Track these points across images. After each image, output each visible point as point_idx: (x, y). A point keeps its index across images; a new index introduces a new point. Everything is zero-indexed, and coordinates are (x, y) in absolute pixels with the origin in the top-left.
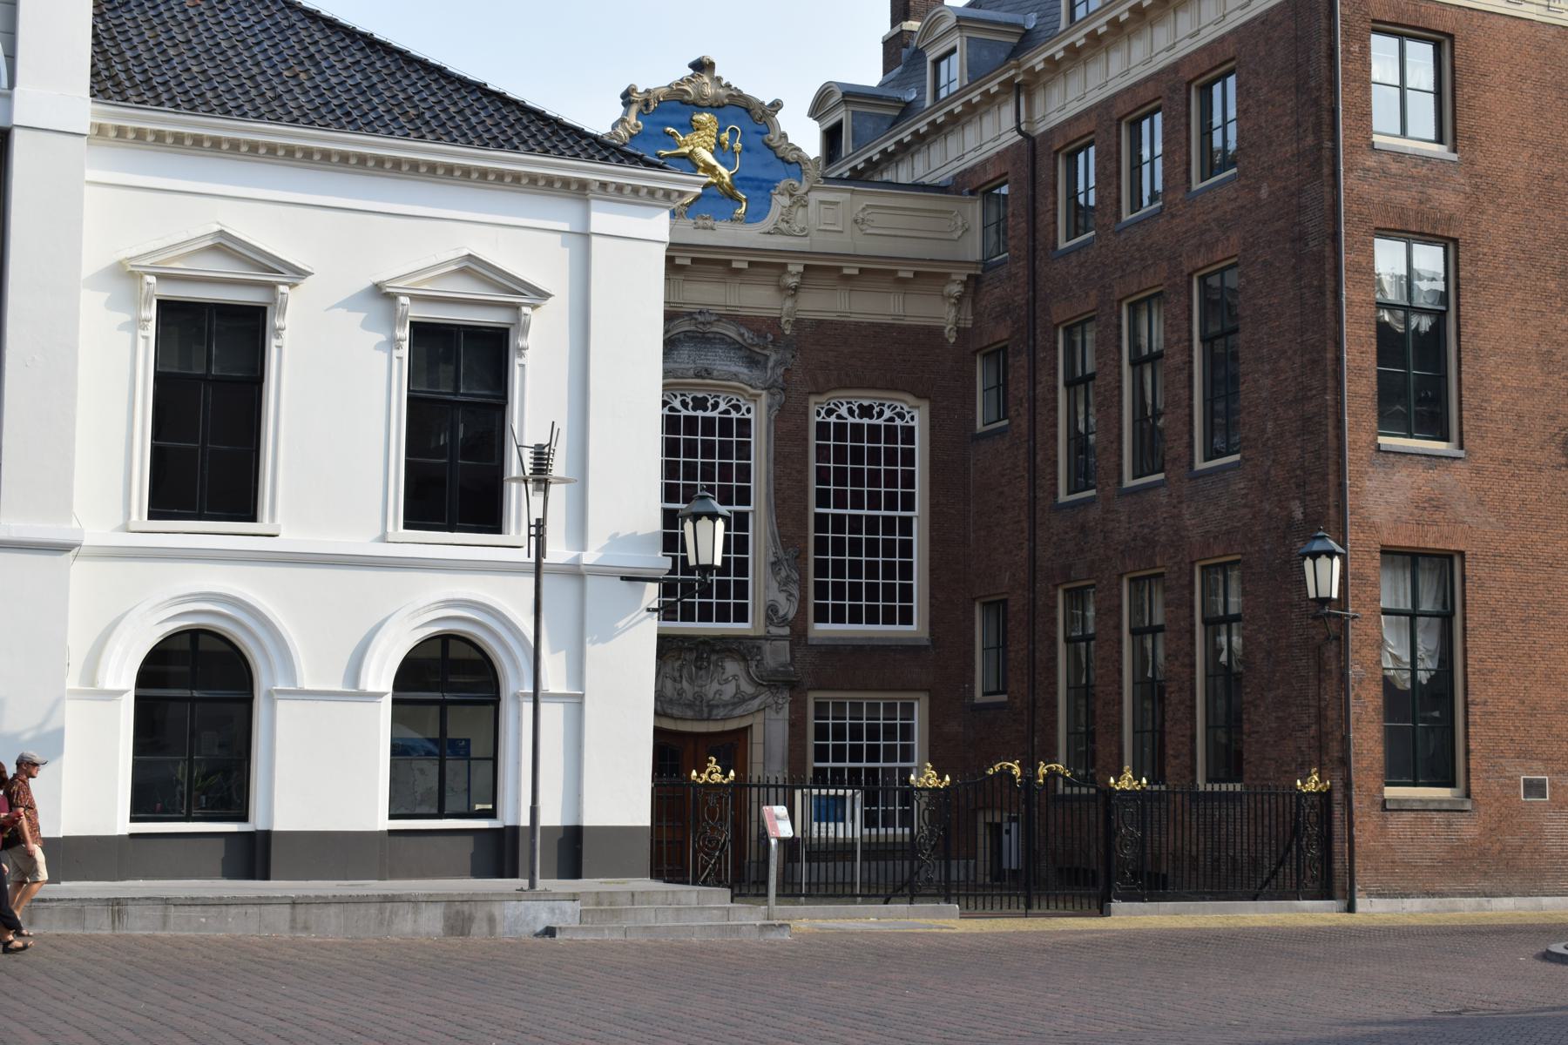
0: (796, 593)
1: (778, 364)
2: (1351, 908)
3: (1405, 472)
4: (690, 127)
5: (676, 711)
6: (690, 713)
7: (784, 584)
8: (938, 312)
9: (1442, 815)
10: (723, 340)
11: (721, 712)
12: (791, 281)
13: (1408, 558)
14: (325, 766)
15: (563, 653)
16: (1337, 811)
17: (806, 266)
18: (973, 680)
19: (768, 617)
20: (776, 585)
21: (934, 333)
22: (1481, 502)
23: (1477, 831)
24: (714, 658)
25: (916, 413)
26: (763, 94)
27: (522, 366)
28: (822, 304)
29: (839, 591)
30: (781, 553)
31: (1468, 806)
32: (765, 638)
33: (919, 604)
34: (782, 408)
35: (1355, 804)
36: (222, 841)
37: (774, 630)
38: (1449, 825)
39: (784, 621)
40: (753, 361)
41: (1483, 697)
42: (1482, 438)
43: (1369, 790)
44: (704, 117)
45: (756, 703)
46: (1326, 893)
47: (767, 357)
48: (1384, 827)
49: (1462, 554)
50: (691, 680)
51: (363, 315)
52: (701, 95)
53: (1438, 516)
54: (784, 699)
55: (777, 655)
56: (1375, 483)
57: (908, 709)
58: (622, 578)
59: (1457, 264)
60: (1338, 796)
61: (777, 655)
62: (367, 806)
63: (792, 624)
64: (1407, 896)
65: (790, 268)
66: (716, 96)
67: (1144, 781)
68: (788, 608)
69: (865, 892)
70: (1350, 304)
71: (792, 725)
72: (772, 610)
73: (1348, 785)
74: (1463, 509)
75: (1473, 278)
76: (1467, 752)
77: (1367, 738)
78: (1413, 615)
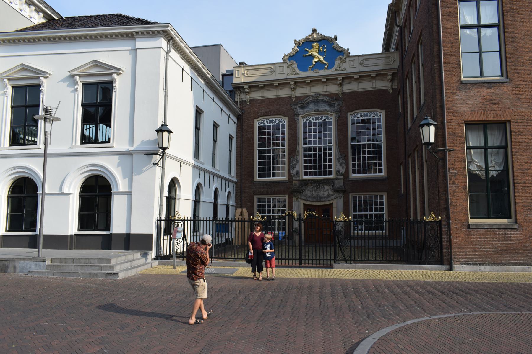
0: (345, 166)
1: (338, 105)
2: (451, 269)
3: (476, 91)
4: (311, 47)
5: (311, 200)
6: (315, 200)
7: (341, 164)
8: (382, 85)
9: (501, 230)
10: (322, 101)
11: (324, 200)
12: (339, 82)
13: (482, 126)
14: (60, 215)
15: (127, 179)
16: (444, 229)
17: (343, 78)
18: (401, 188)
19: (337, 173)
20: (339, 165)
21: (385, 91)
22: (519, 99)
23: (521, 237)
24: (321, 185)
25: (381, 114)
26: (330, 34)
27: (115, 92)
28: (350, 87)
29: (359, 165)
30: (340, 156)
31: (516, 226)
32: (336, 179)
33: (384, 168)
34: (339, 116)
35: (452, 227)
36: (101, 237)
37: (338, 177)
38: (505, 235)
39: (341, 174)
40: (331, 106)
41: (523, 180)
42: (519, 73)
43: (461, 220)
44: (315, 44)
45: (333, 196)
46: (440, 262)
47: (335, 104)
48: (469, 236)
49: (509, 121)
50: (315, 191)
51: (67, 83)
52: (314, 39)
53: (495, 107)
54: (341, 195)
55: (340, 183)
56: (460, 97)
57: (381, 197)
58: (145, 154)
59: (502, 5)
60: (444, 223)
61: (340, 183)
62: (71, 227)
63: (343, 175)
64: (483, 264)
65: (338, 79)
66: (318, 38)
67: (350, 217)
68: (342, 171)
69: (217, 256)
70: (444, 28)
71: (344, 202)
72: (338, 172)
73: (448, 218)
74: (509, 103)
75: (509, 11)
76: (515, 204)
77: (460, 197)
78: (486, 148)
